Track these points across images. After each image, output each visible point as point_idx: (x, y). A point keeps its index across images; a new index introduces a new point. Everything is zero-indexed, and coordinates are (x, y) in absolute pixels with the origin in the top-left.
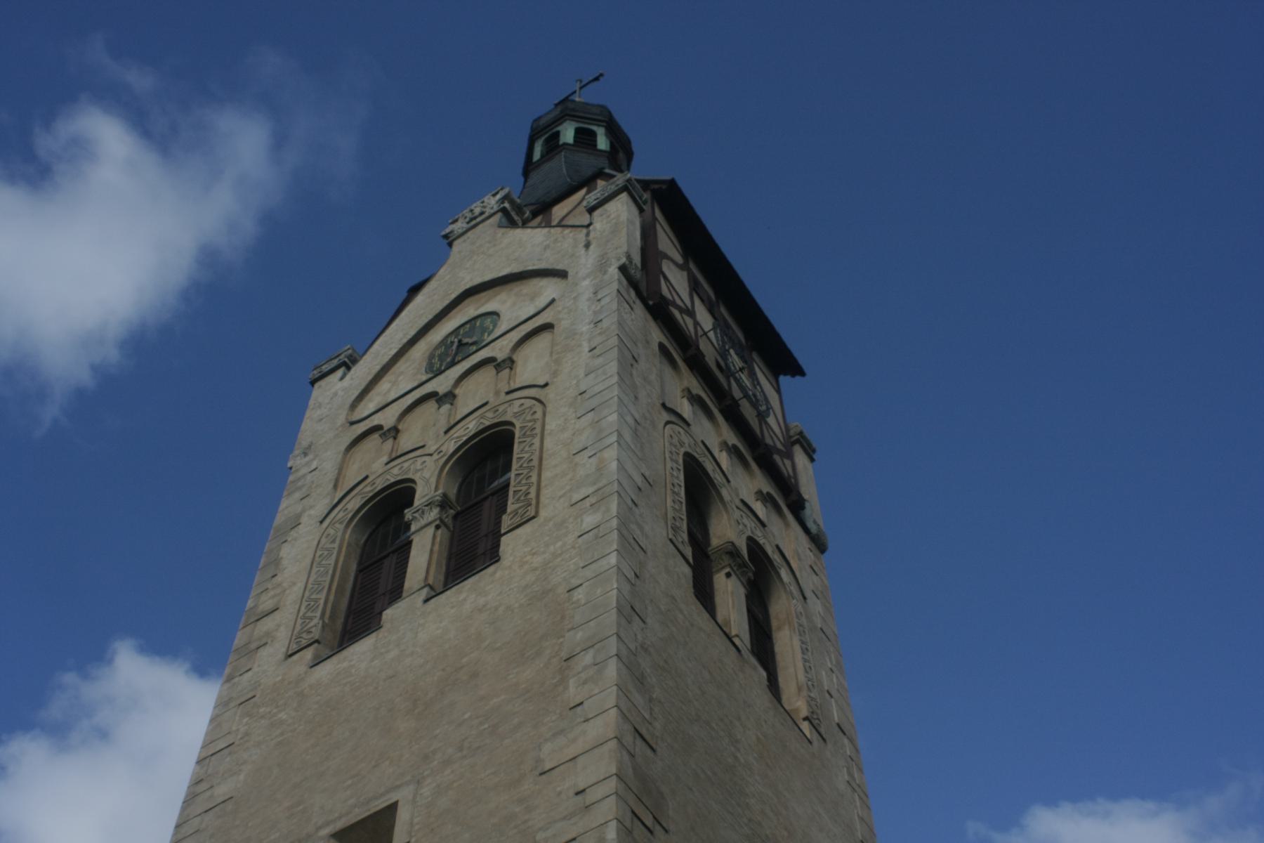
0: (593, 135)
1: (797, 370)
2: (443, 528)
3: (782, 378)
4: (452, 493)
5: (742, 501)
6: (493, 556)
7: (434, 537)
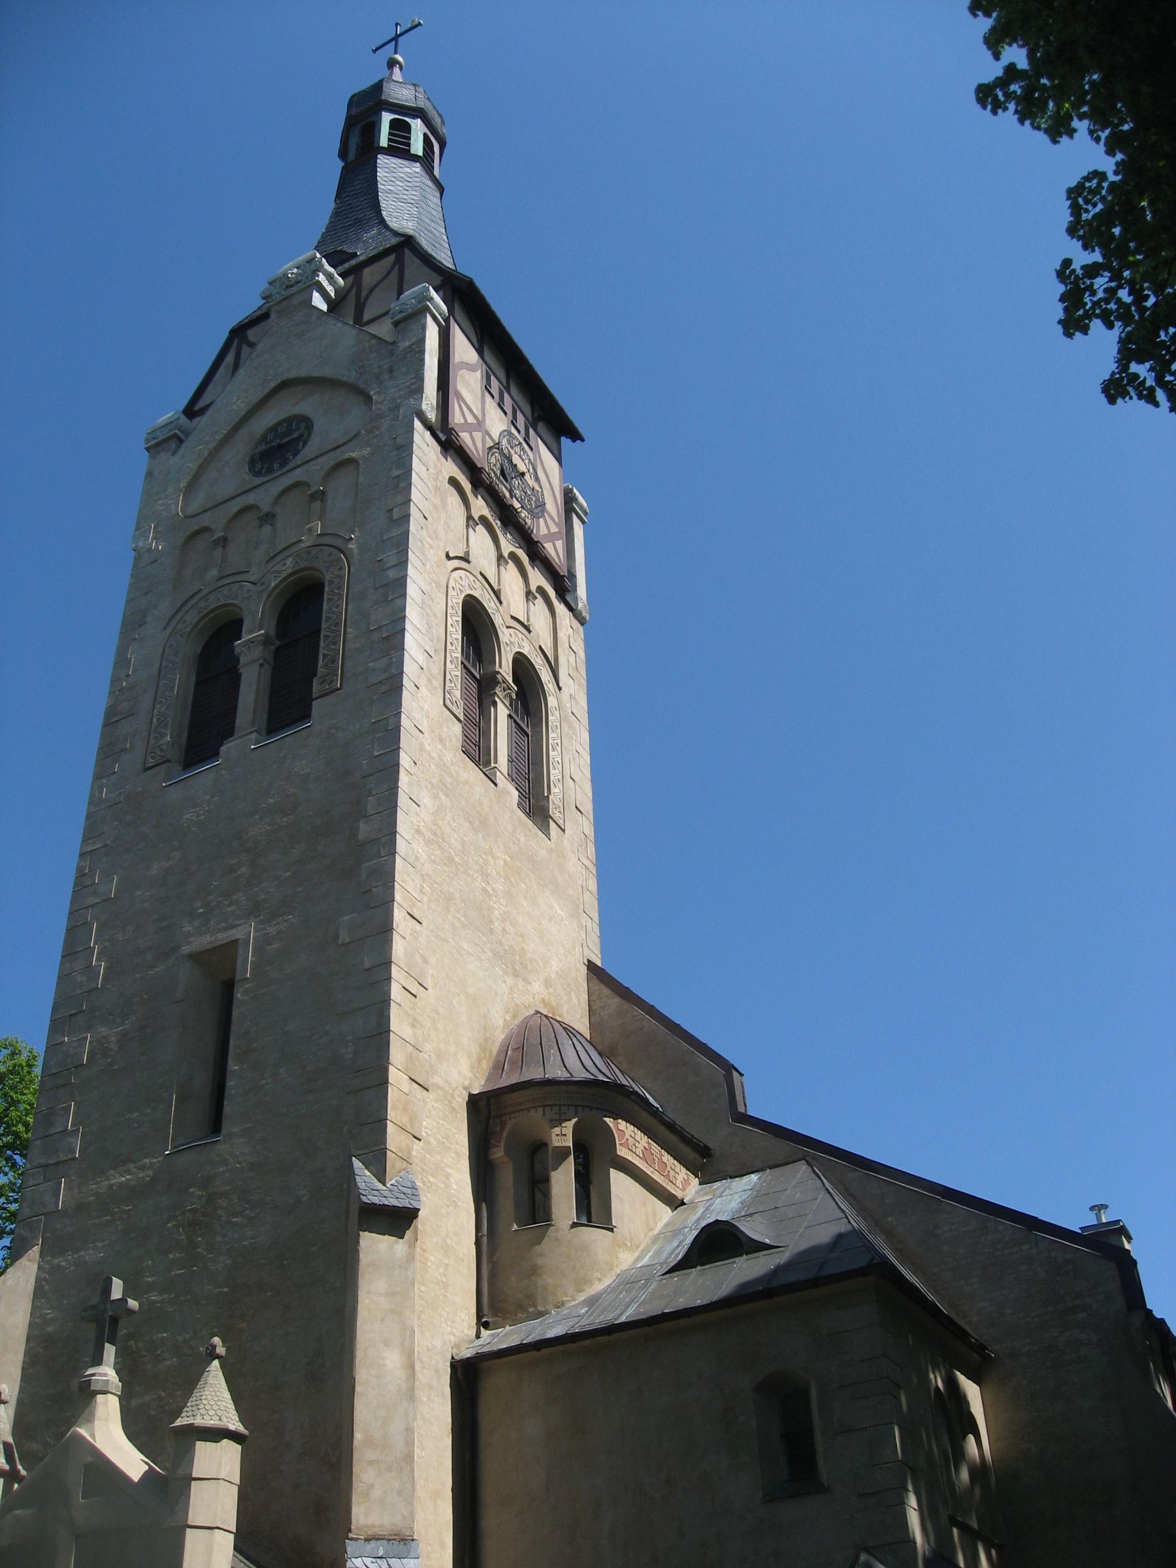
0: (407, 128)
1: (575, 436)
2: (267, 666)
3: (563, 439)
4: (273, 633)
5: (513, 618)
6: (306, 715)
7: (259, 674)
